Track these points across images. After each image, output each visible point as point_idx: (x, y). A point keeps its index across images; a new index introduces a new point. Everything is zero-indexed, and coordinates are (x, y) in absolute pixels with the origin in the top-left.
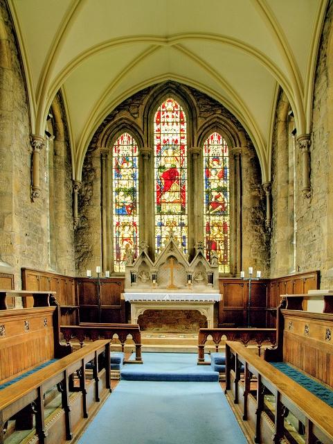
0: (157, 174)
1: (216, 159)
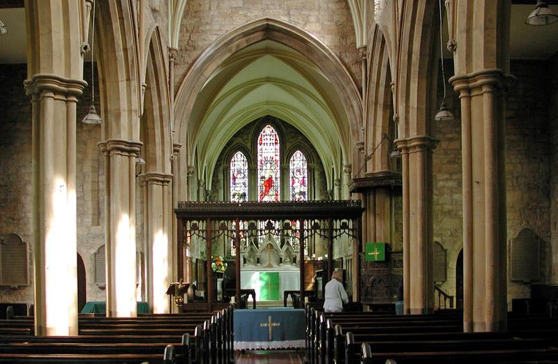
0: (260, 182)
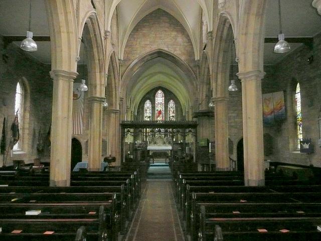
0: (156, 112)
1: (172, 107)
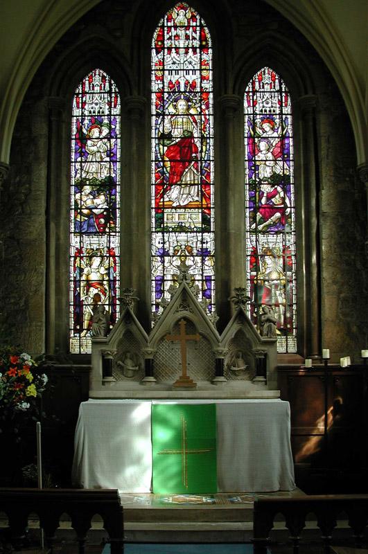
1: (269, 118)
